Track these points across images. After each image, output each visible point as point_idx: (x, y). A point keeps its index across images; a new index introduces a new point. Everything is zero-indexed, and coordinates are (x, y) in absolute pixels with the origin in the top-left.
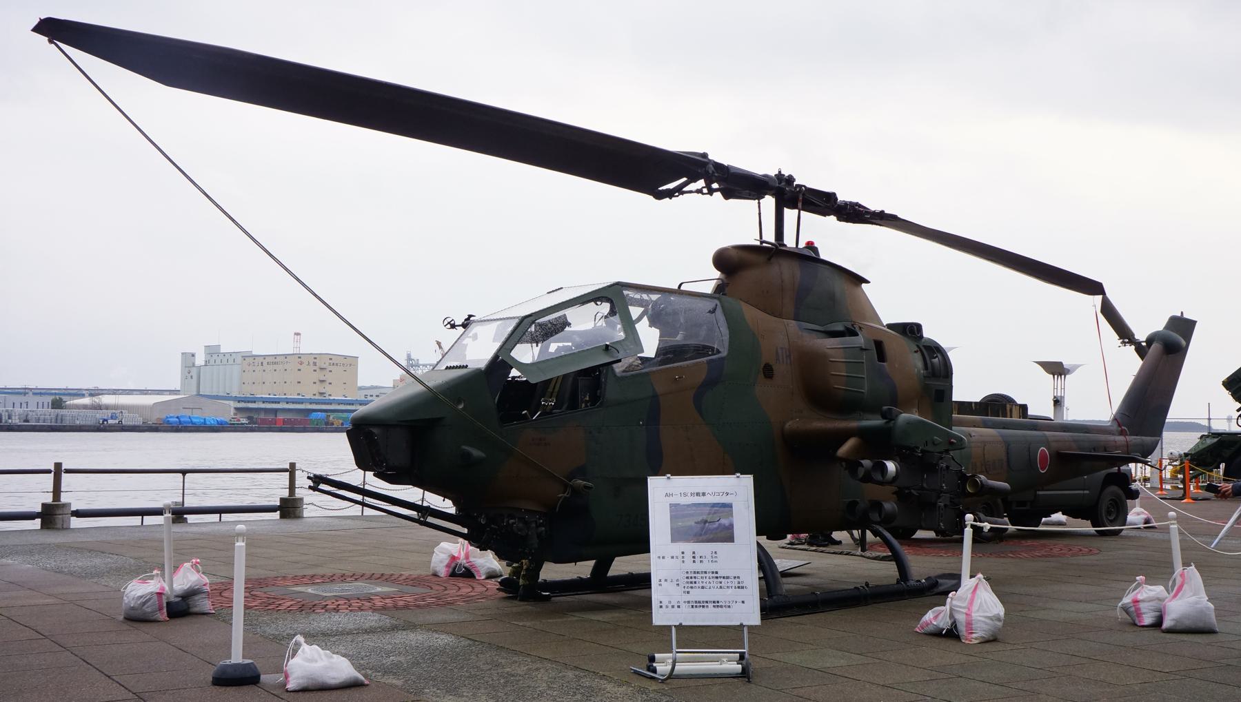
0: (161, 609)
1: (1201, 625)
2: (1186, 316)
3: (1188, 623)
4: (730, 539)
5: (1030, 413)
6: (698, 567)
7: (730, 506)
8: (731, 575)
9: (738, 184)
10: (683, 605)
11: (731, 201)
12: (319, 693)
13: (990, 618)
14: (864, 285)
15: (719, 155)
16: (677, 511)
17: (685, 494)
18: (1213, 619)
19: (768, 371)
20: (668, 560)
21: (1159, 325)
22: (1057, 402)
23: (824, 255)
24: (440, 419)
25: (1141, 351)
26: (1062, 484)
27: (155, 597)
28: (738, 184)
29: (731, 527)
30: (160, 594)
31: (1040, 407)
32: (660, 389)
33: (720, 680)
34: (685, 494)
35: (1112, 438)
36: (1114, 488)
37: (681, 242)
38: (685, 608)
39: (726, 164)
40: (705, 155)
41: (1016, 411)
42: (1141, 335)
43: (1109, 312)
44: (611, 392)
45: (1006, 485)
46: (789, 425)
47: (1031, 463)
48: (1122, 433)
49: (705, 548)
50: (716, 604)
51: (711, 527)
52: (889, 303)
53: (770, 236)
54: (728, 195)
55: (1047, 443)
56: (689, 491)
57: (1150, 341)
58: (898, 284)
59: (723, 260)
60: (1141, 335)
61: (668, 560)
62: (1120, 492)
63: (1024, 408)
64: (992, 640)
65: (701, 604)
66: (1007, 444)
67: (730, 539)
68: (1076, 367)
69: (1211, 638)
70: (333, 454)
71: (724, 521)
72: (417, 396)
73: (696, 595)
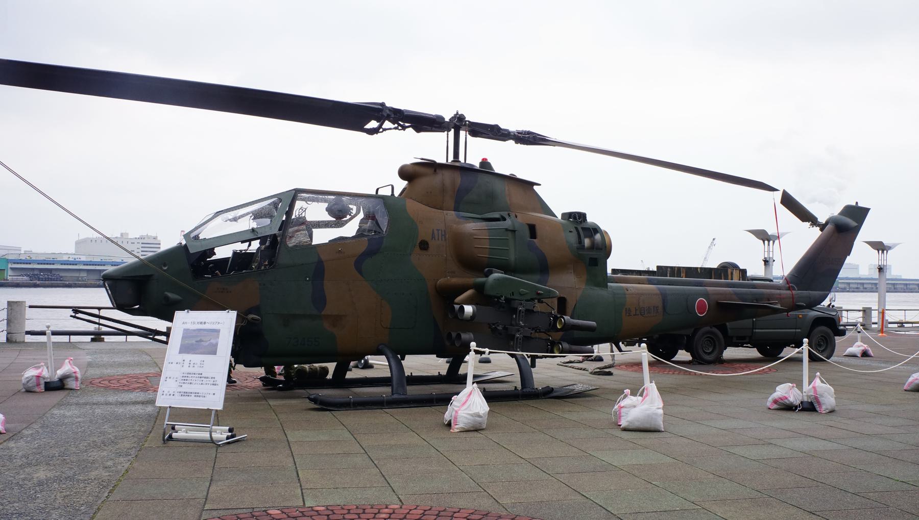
0: (38, 385)
1: (647, 426)
2: (860, 205)
3: (637, 425)
4: (214, 353)
5: (749, 274)
6: (191, 370)
7: (218, 331)
8: (210, 375)
9: (424, 123)
10: (176, 394)
11: (423, 134)
12: (642, 434)
13: (471, 415)
14: (535, 187)
15: (393, 102)
16: (187, 334)
17: (194, 323)
18: (661, 424)
19: (424, 246)
20: (174, 364)
21: (835, 211)
22: (881, 269)
23: (498, 169)
24: (151, 275)
25: (822, 227)
26: (717, 323)
27: (34, 378)
28: (424, 123)
29: (217, 344)
30: (38, 377)
31: (755, 269)
32: (323, 258)
33: (192, 444)
34: (194, 323)
35: (782, 292)
36: (824, 328)
37: (373, 165)
38: (177, 396)
39: (402, 108)
40: (383, 104)
41: (736, 274)
42: (822, 220)
43: (788, 202)
44: (283, 258)
45: (594, 323)
46: (442, 281)
47: (689, 309)
48: (789, 289)
49: (196, 358)
50: (197, 395)
51: (197, 344)
52: (559, 199)
53: (451, 158)
54: (418, 130)
55: (706, 295)
56: (196, 321)
57: (827, 223)
58: (563, 186)
59: (404, 173)
60: (822, 220)
61: (174, 364)
62: (829, 331)
63: (744, 272)
64: (475, 429)
65: (186, 394)
66: (664, 296)
67: (214, 353)
68: (895, 245)
69: (661, 435)
70: (100, 297)
71: (213, 341)
72: (135, 263)
73: (186, 388)
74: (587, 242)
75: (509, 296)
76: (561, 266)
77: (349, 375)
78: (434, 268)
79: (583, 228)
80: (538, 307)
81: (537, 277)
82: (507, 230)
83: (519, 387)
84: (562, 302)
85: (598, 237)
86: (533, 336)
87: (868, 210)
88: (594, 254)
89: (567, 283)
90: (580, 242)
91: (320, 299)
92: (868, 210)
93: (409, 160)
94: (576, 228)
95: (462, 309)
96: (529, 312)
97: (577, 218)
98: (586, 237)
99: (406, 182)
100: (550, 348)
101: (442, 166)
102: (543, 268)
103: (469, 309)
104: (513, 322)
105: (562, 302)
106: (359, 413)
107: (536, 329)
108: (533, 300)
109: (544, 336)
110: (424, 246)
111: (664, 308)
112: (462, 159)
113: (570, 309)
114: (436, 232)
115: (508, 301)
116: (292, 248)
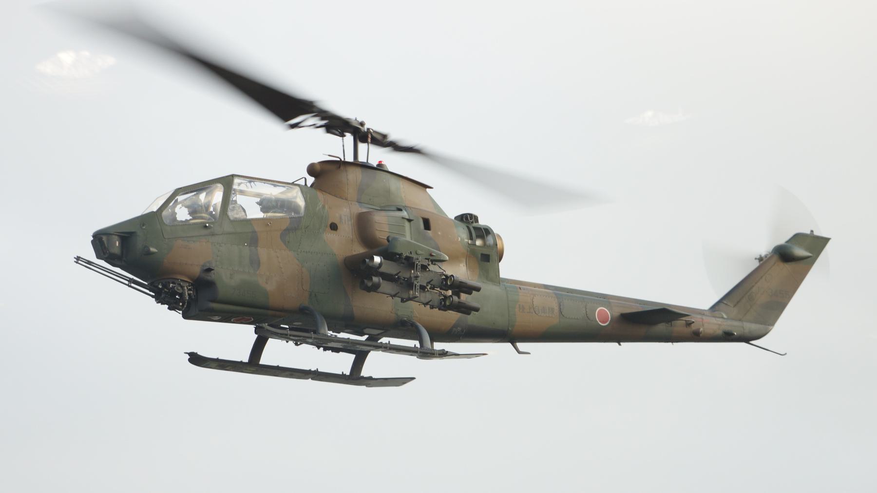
2: (816, 233)
78: (342, 244)
79: (475, 228)
87: (826, 240)
88: (486, 252)
91: (255, 262)
92: (826, 240)
94: (468, 227)
110: (334, 227)
111: (561, 312)
115: (408, 258)
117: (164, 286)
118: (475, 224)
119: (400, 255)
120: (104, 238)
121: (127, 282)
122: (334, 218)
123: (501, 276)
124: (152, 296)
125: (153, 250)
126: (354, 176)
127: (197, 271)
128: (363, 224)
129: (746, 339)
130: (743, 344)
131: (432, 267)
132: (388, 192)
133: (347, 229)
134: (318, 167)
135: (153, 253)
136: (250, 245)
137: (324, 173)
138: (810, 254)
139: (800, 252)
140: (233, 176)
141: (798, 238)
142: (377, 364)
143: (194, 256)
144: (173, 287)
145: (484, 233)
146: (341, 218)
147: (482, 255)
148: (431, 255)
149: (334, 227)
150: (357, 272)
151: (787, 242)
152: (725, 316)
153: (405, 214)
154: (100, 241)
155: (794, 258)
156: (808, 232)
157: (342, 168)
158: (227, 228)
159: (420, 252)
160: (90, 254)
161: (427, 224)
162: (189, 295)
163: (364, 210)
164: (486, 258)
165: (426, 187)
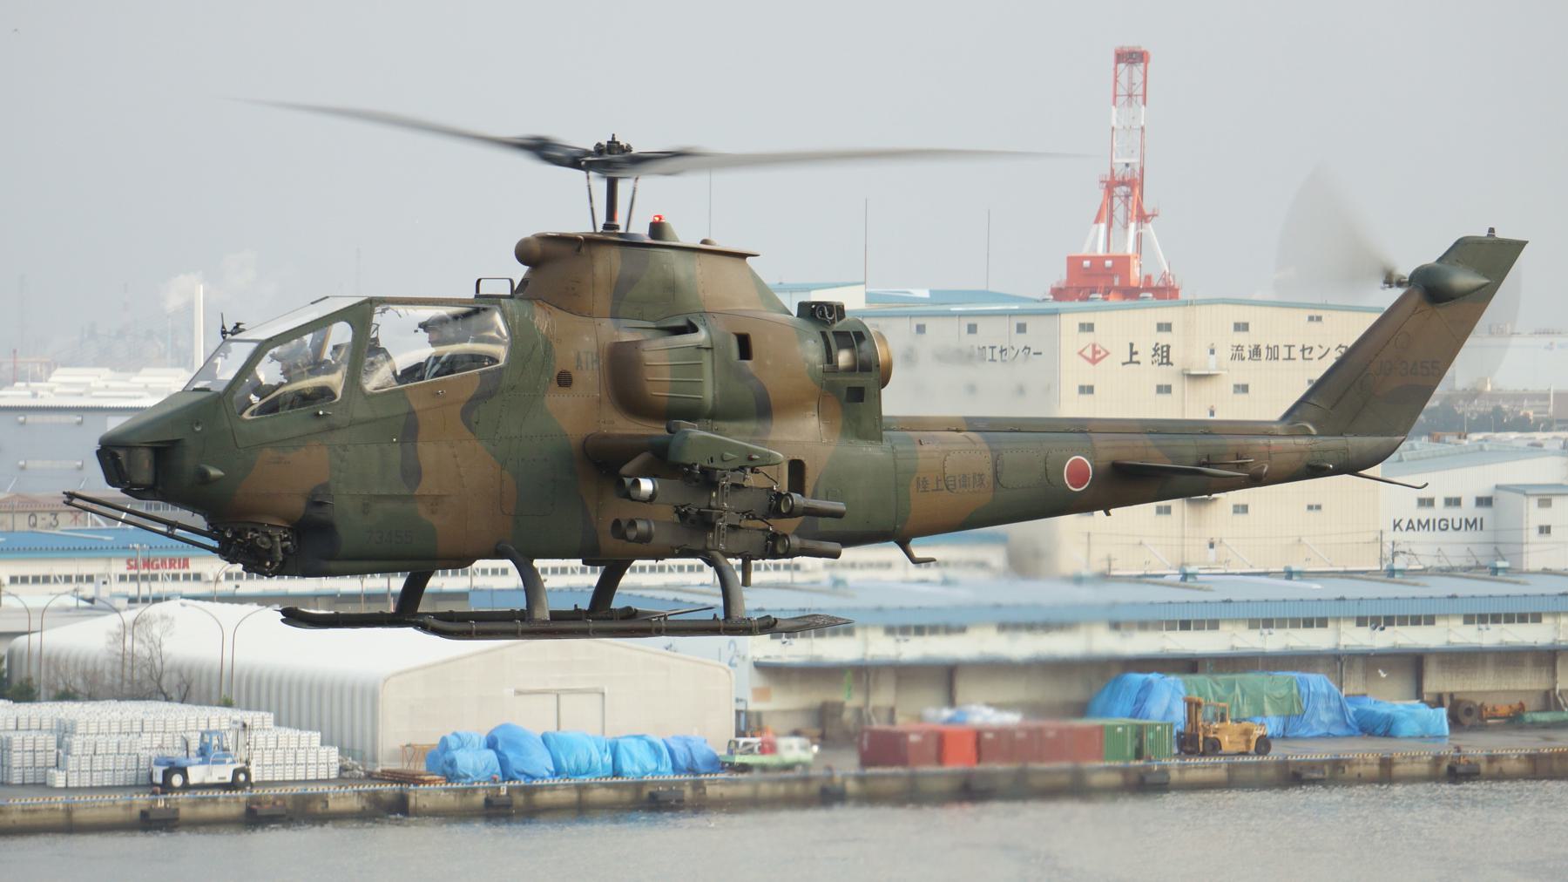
2: (1499, 235)
74: (843, 358)
75: (705, 464)
76: (793, 406)
77: (397, 583)
78: (578, 413)
79: (836, 333)
80: (752, 480)
81: (751, 426)
82: (699, 348)
83: (721, 616)
84: (797, 468)
85: (865, 346)
86: (743, 524)
87: (1521, 245)
88: (857, 380)
89: (804, 435)
90: (830, 358)
91: (412, 473)
92: (1521, 245)
93: (529, 232)
94: (824, 334)
95: (637, 484)
96: (737, 487)
97: (818, 314)
98: (840, 347)
99: (526, 268)
100: (774, 548)
101: (590, 241)
102: (763, 409)
103: (646, 485)
104: (713, 504)
105: (797, 468)
106: (738, 820)
107: (750, 515)
108: (742, 468)
109: (762, 525)
110: (565, 380)
111: (996, 474)
112: (621, 220)
113: (809, 484)
114: (583, 358)
115: (705, 471)
116: (372, 396)
117: (236, 534)
118: (838, 326)
119: (691, 466)
120: (121, 454)
121: (164, 529)
122: (564, 358)
123: (885, 412)
124: (213, 550)
125: (214, 472)
126: (609, 263)
127: (298, 506)
128: (622, 373)
129: (1352, 467)
130: (1346, 478)
131: (752, 480)
132: (671, 287)
133: (590, 379)
134: (537, 248)
135: (217, 479)
136: (402, 442)
137: (547, 258)
138: (1485, 281)
139: (1464, 279)
140: (372, 303)
141: (1464, 251)
142: (644, 582)
143: (290, 473)
144: (253, 540)
145: (856, 338)
146: (578, 359)
147: (850, 389)
148: (750, 459)
149: (565, 380)
150: (604, 463)
151: (1440, 260)
152: (1313, 431)
153: (701, 337)
154: (113, 456)
155: (1447, 296)
156: (1484, 233)
157: (583, 250)
158: (361, 412)
159: (729, 455)
160: (95, 483)
161: (745, 346)
162: (284, 550)
163: (627, 337)
164: (857, 395)
165: (743, 256)
